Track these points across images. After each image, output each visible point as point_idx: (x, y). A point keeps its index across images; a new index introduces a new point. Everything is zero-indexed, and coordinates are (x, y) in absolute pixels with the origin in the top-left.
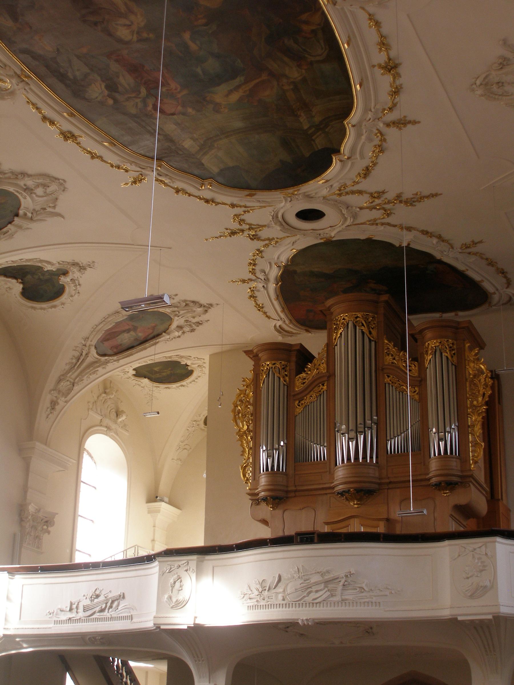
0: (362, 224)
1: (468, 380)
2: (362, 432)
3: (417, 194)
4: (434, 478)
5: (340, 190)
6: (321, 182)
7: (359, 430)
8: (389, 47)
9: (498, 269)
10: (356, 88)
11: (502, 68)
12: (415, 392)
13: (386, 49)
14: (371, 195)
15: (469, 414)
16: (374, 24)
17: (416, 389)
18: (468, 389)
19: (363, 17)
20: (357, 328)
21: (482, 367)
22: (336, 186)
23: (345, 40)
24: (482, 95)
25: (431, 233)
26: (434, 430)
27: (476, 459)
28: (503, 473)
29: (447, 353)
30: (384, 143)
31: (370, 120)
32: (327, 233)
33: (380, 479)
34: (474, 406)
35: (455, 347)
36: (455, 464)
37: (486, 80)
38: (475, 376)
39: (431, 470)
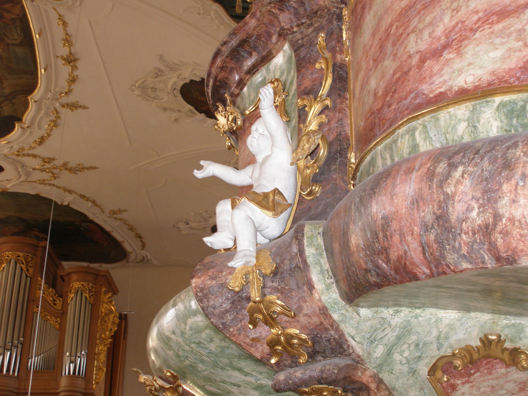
0: (33, 182)
1: (100, 317)
2: (9, 349)
3: (79, 165)
4: (62, 393)
5: (18, 151)
6: (3, 143)
7: (7, 347)
8: (72, 44)
9: (137, 234)
10: (41, 72)
11: (156, 77)
12: (57, 322)
13: (69, 45)
14: (43, 160)
15: (97, 344)
16: (62, 23)
17: (58, 319)
18: (99, 324)
19: (54, 16)
20: (18, 265)
21: (113, 308)
22: (16, 147)
23: (37, 32)
24: (139, 96)
25: (87, 198)
26: (68, 354)
27: (97, 380)
28: (120, 390)
29: (86, 294)
30: (58, 120)
31: (49, 99)
32: (4, 185)
33: (18, 389)
34: (102, 338)
35: (94, 290)
36: (81, 383)
37: (144, 84)
38: (106, 314)
39: (61, 386)
